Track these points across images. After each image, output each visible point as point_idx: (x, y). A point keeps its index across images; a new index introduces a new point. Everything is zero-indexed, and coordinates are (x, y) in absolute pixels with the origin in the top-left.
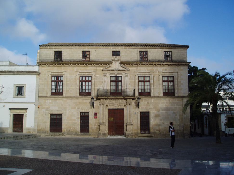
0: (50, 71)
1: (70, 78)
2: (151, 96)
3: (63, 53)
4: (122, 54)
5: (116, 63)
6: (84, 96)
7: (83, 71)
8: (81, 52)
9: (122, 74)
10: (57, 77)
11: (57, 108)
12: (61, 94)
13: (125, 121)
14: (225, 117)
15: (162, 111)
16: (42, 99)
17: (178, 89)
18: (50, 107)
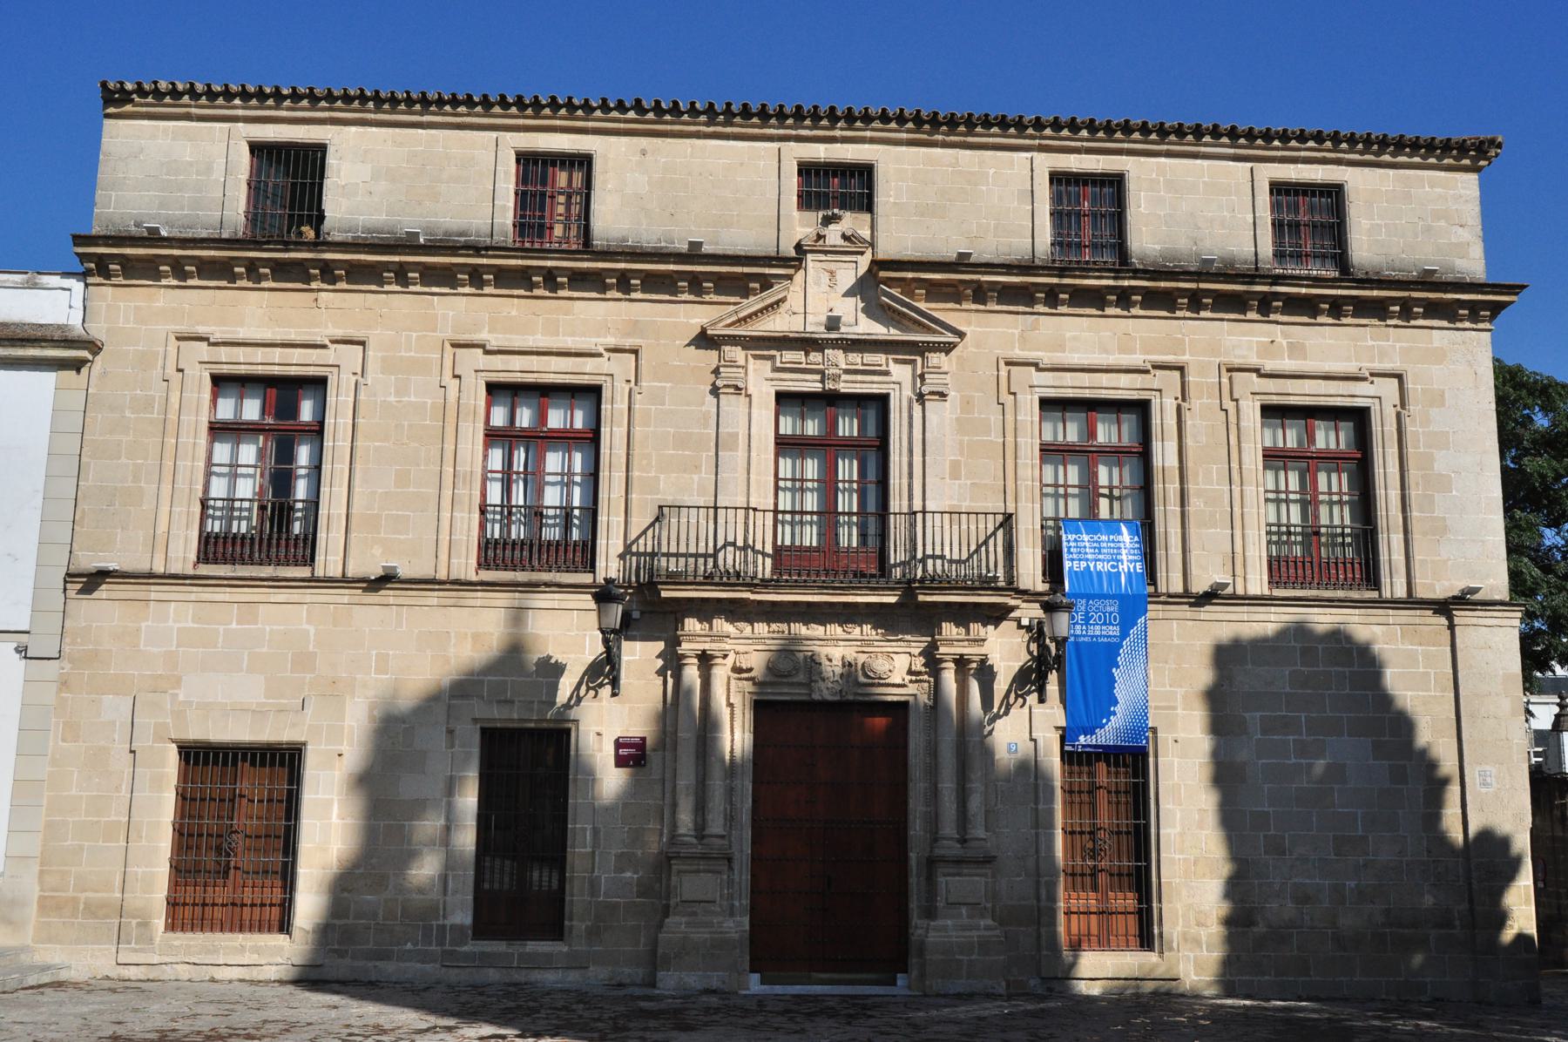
1: (392, 399)
3: (331, 160)
4: (886, 193)
5: (832, 273)
7: (518, 342)
8: (510, 167)
9: (887, 373)
10: (285, 391)
11: (252, 690)
12: (306, 549)
13: (917, 828)
15: (1264, 732)
16: (435, 601)
18: (178, 682)
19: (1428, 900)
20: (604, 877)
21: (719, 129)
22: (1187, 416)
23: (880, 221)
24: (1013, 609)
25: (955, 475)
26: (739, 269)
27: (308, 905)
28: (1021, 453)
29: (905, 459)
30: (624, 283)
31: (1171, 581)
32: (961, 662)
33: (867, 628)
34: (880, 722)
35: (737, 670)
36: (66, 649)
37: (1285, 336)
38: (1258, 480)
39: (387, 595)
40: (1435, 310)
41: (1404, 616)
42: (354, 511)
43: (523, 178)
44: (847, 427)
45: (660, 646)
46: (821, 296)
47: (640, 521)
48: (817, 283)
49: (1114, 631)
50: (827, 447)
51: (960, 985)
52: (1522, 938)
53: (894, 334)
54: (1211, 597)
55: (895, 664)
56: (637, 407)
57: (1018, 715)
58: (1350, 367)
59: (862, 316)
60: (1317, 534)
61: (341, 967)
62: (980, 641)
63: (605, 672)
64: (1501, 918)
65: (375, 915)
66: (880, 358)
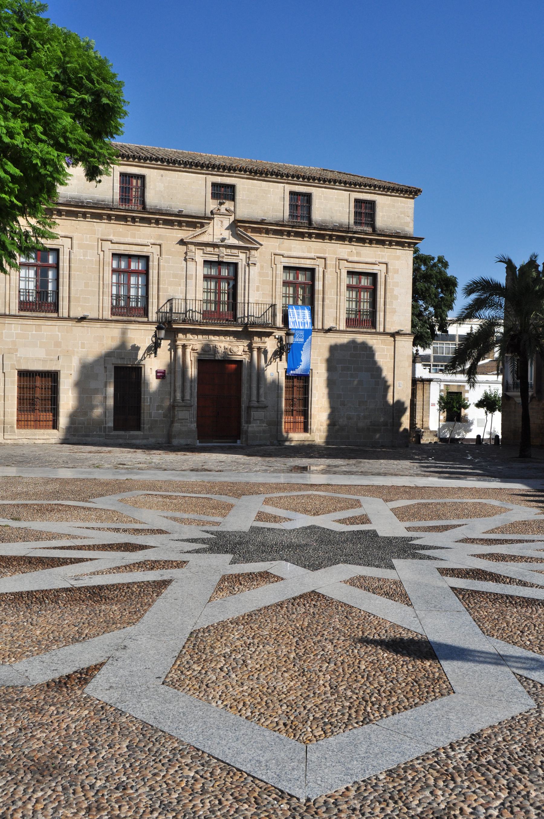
1: (82, 258)
4: (240, 195)
5: (222, 222)
7: (122, 241)
9: (238, 256)
11: (41, 353)
12: (56, 307)
13: (244, 398)
14: (441, 391)
18: (17, 350)
19: (382, 419)
20: (154, 412)
21: (187, 170)
22: (326, 274)
23: (237, 205)
24: (273, 333)
25: (258, 290)
26: (194, 220)
27: (63, 421)
28: (277, 284)
29: (243, 284)
30: (157, 222)
31: (319, 325)
32: (259, 349)
33: (231, 337)
34: (233, 366)
35: (193, 350)
37: (356, 249)
38: (345, 293)
39: (84, 324)
40: (398, 244)
41: (382, 337)
42: (72, 295)
43: (122, 182)
44: (225, 272)
45: (169, 342)
46: (218, 230)
47: (163, 301)
48: (217, 225)
49: (302, 340)
50: (218, 279)
51: (257, 442)
52: (405, 430)
53: (241, 244)
54: (329, 330)
55: (239, 349)
56: (161, 264)
57: (274, 364)
58: (373, 260)
59: (231, 237)
60: (360, 311)
61: (75, 439)
62: (265, 343)
63: (154, 348)
64: (400, 424)
65: (84, 424)
66: (236, 251)
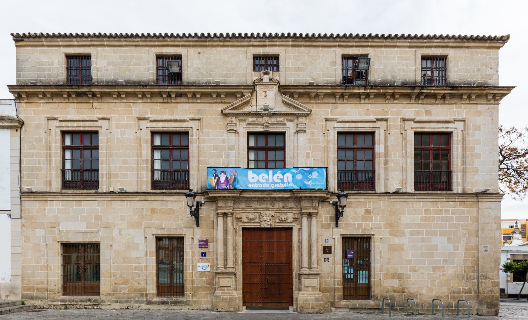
0: (55, 116)
1: (120, 137)
2: (455, 191)
6: (178, 191)
7: (160, 117)
9: (285, 124)
11: (82, 226)
15: (411, 235)
17: (464, 171)
18: (59, 224)
20: (197, 279)
24: (328, 198)
36: (23, 215)
37: (424, 108)
66: (282, 119)
